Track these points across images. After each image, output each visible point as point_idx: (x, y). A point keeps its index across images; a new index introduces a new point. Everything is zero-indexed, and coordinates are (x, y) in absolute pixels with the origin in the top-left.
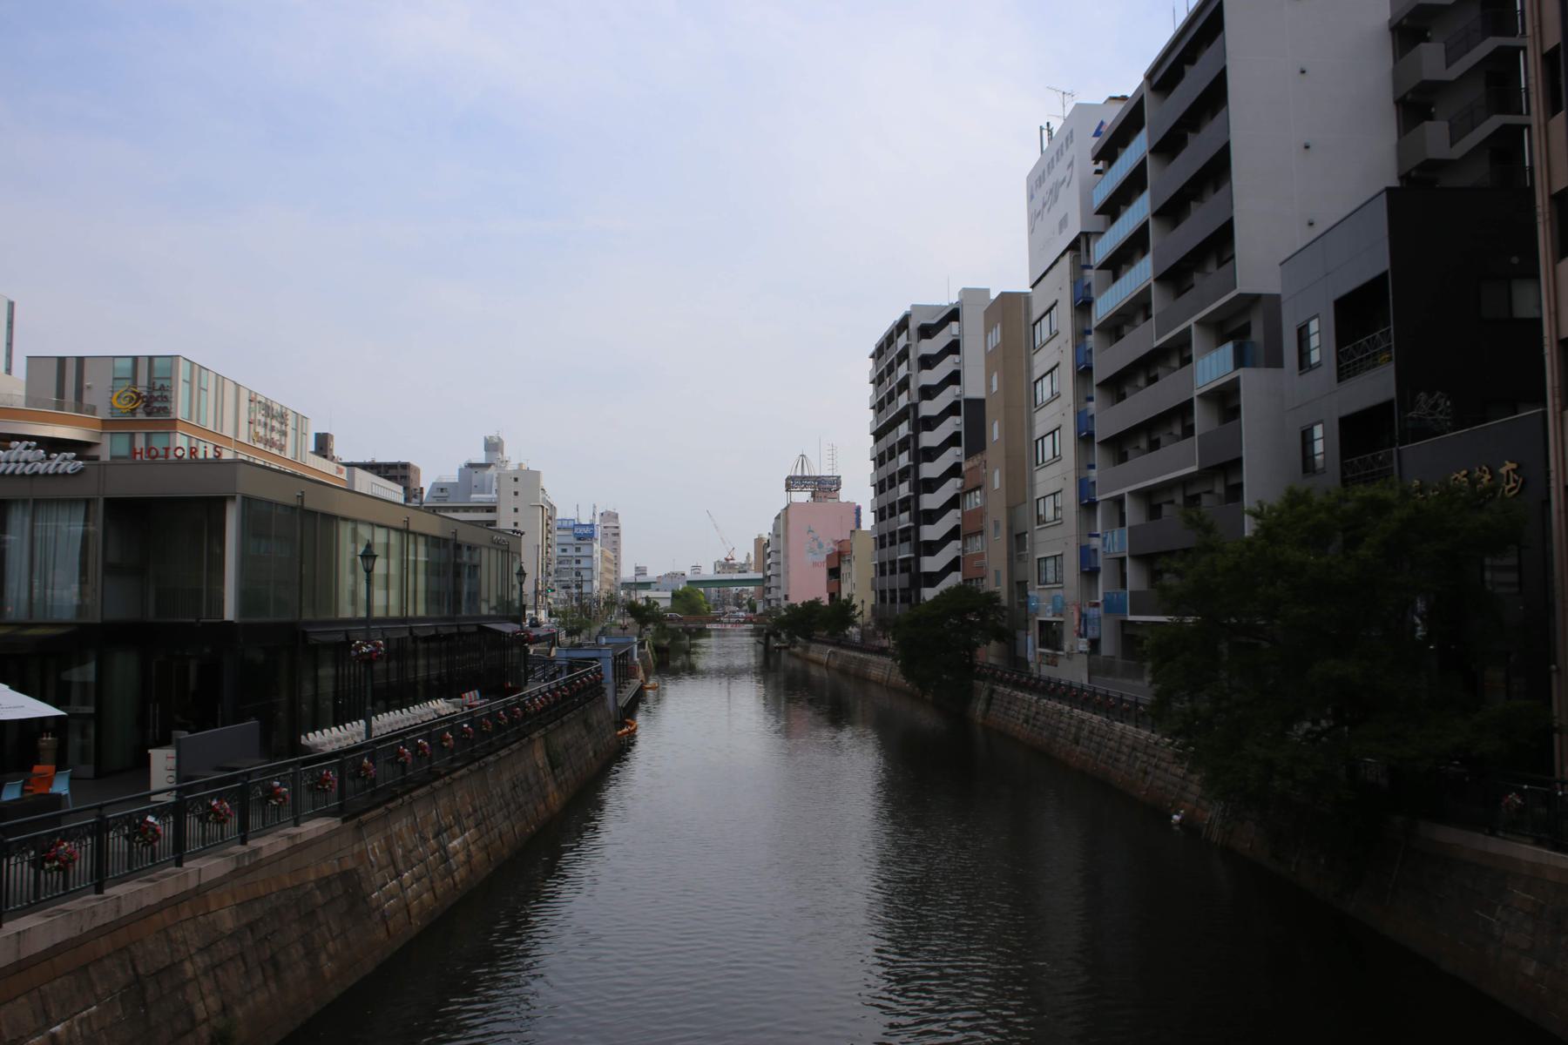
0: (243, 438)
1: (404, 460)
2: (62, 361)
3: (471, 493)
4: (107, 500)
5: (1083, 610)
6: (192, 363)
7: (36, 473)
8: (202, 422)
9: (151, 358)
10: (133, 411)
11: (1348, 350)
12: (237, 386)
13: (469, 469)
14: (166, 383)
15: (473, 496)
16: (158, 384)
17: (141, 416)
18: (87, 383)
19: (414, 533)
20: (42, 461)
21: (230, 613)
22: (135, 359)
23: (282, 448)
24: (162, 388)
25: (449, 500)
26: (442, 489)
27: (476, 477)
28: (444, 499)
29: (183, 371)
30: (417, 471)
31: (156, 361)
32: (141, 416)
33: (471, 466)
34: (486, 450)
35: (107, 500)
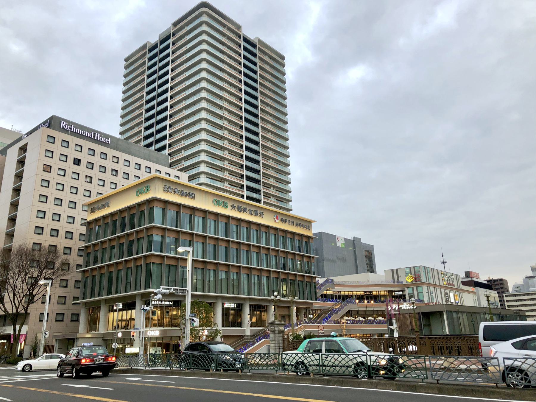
0: (442, 284)
1: (500, 278)
2: (392, 270)
3: (529, 288)
4: (422, 313)
5: (156, 322)
6: (425, 267)
7: (409, 309)
8: (430, 282)
9: (414, 267)
10: (412, 282)
11: (415, 320)
12: (438, 270)
13: (528, 279)
14: (419, 273)
15: (530, 289)
16: (417, 273)
17: (414, 282)
18: (399, 275)
19: (461, 312)
20: (409, 306)
21: (448, 333)
22: (410, 268)
23: (453, 285)
24: (418, 275)
25: (521, 291)
26: (518, 287)
27: (531, 281)
28: (519, 291)
29: (422, 270)
30: (506, 281)
31: (416, 268)
32: (414, 282)
33: (527, 277)
34: (532, 271)
35: (422, 313)
